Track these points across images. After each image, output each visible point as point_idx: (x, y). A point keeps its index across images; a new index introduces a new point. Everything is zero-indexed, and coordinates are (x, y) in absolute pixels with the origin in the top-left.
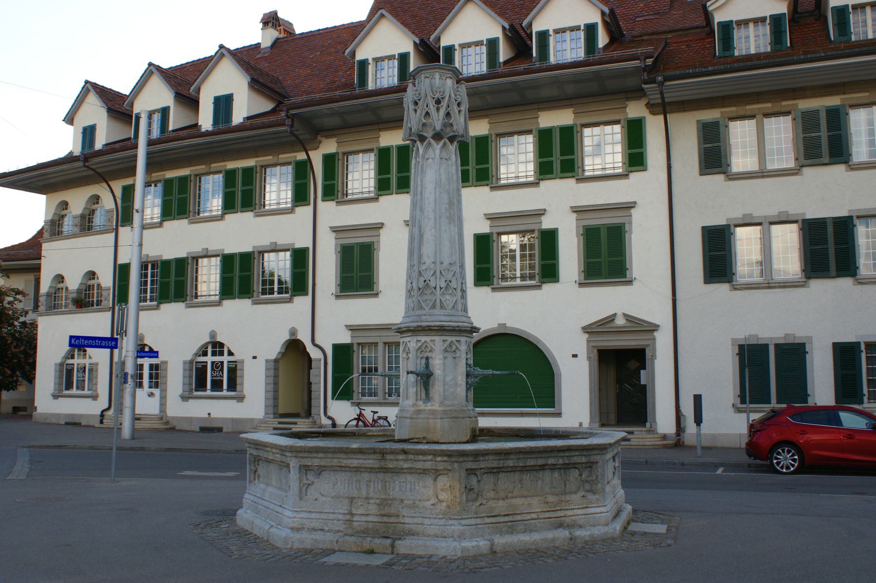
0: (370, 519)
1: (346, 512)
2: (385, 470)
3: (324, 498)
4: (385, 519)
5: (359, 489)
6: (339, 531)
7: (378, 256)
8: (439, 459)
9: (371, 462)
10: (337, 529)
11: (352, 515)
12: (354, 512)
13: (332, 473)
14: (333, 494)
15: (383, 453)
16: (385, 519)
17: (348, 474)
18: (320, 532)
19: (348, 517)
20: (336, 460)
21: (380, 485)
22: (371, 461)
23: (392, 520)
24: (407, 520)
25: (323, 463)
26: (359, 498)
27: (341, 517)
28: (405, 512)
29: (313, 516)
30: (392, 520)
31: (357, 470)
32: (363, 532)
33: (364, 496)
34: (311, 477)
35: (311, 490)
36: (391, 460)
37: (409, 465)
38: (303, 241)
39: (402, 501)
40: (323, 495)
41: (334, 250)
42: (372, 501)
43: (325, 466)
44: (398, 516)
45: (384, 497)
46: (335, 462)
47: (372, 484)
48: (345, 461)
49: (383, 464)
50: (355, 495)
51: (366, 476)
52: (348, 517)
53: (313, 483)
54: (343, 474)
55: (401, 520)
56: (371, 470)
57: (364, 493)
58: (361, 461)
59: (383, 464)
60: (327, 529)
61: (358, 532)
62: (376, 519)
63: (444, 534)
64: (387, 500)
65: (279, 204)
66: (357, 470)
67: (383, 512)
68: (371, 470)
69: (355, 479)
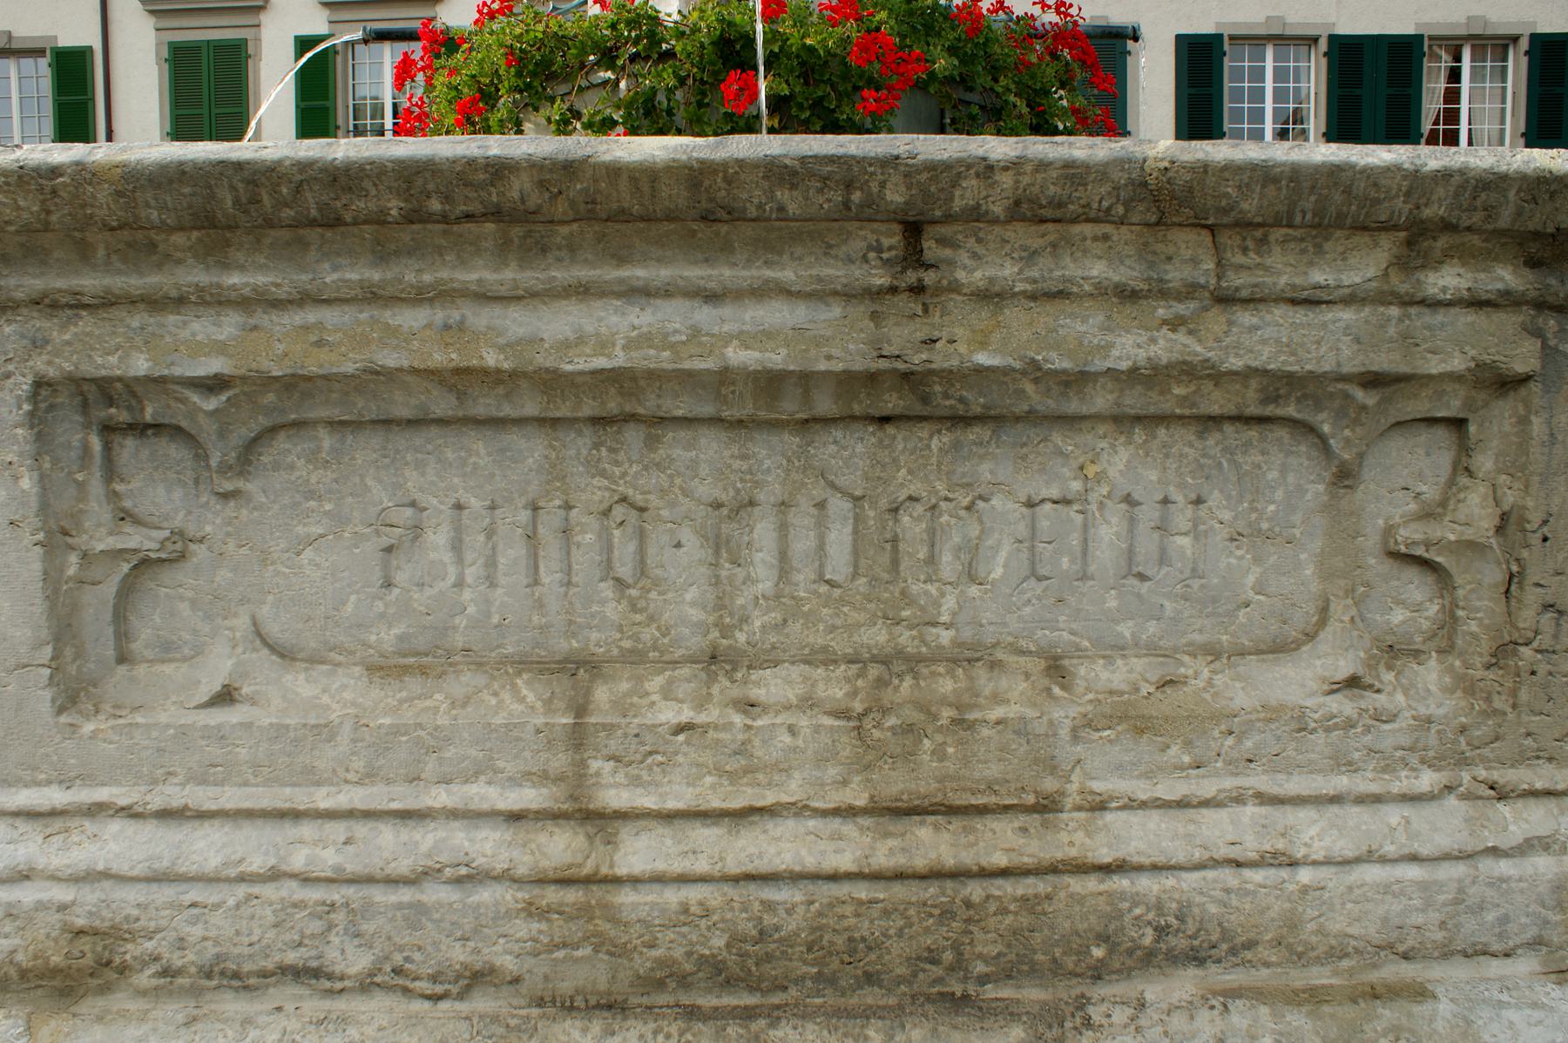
0: (781, 846)
1: (529, 797)
2: (905, 401)
3: (301, 684)
4: (932, 844)
5: (637, 584)
6: (477, 978)
7: (257, 72)
8: (1447, 280)
9: (767, 322)
10: (459, 955)
11: (600, 822)
12: (615, 797)
13: (365, 450)
14: (386, 637)
15: (917, 229)
16: (932, 844)
17: (532, 450)
18: (287, 993)
19: (560, 847)
20: (411, 318)
21: (839, 538)
22: (778, 314)
23: (1000, 841)
24: (1137, 835)
25: (280, 344)
26: (635, 657)
27: (488, 846)
28: (1104, 767)
29: (206, 847)
30: (1000, 841)
31: (619, 407)
32: (719, 974)
33: (696, 643)
34: (160, 491)
35: (168, 607)
36: (992, 296)
37: (1165, 347)
38: (79, 32)
39: (1056, 669)
40: (285, 654)
41: (153, 55)
42: (772, 686)
43: (295, 384)
44: (1046, 806)
45: (877, 636)
46: (410, 336)
47: (763, 531)
48: (516, 322)
49: (903, 335)
50: (596, 640)
51: (704, 463)
52: (560, 847)
53: (176, 551)
54: (480, 448)
55: (1072, 838)
56: (769, 404)
57: (685, 608)
58: (673, 316)
59: (903, 335)
60: (357, 962)
61: (664, 978)
62: (845, 848)
63: (1471, 929)
64: (913, 663)
65: (247, 1022)
66: (619, 407)
67: (896, 784)
68: (769, 404)
69: (595, 492)
